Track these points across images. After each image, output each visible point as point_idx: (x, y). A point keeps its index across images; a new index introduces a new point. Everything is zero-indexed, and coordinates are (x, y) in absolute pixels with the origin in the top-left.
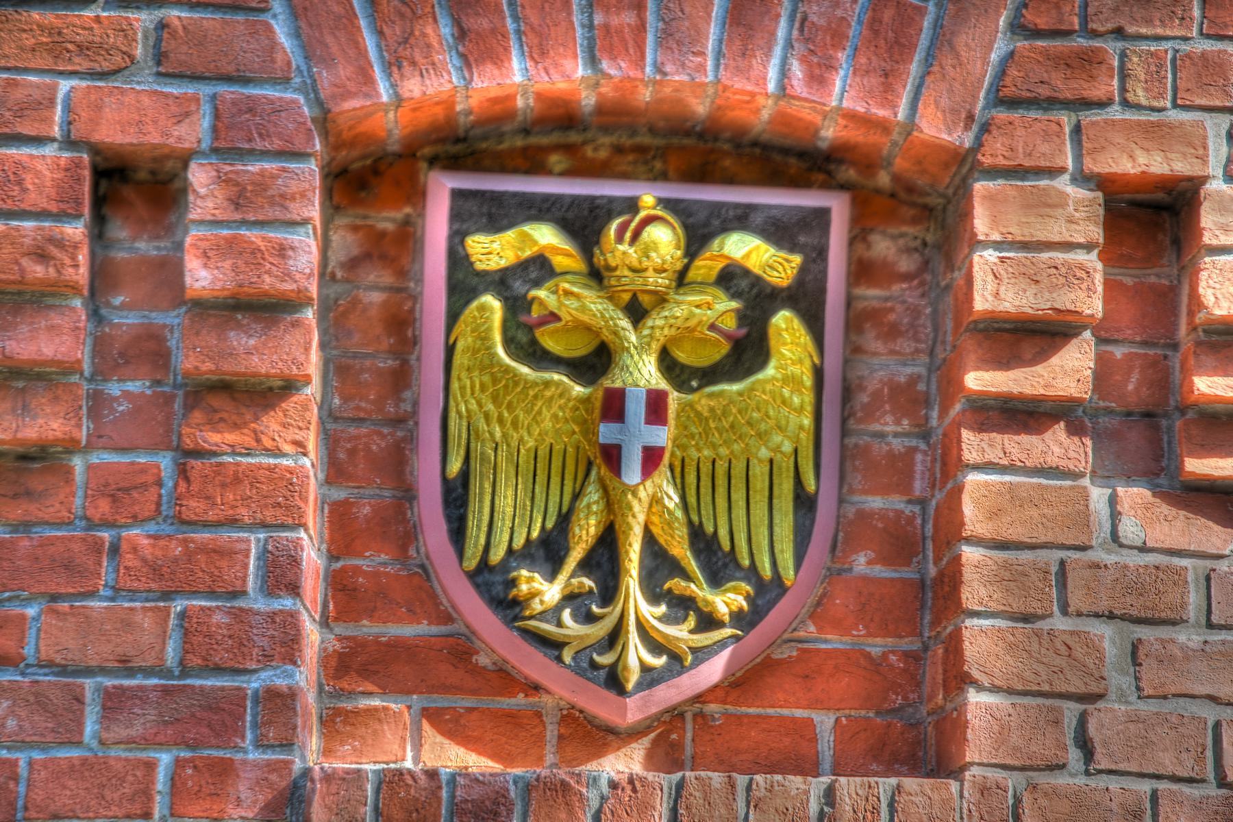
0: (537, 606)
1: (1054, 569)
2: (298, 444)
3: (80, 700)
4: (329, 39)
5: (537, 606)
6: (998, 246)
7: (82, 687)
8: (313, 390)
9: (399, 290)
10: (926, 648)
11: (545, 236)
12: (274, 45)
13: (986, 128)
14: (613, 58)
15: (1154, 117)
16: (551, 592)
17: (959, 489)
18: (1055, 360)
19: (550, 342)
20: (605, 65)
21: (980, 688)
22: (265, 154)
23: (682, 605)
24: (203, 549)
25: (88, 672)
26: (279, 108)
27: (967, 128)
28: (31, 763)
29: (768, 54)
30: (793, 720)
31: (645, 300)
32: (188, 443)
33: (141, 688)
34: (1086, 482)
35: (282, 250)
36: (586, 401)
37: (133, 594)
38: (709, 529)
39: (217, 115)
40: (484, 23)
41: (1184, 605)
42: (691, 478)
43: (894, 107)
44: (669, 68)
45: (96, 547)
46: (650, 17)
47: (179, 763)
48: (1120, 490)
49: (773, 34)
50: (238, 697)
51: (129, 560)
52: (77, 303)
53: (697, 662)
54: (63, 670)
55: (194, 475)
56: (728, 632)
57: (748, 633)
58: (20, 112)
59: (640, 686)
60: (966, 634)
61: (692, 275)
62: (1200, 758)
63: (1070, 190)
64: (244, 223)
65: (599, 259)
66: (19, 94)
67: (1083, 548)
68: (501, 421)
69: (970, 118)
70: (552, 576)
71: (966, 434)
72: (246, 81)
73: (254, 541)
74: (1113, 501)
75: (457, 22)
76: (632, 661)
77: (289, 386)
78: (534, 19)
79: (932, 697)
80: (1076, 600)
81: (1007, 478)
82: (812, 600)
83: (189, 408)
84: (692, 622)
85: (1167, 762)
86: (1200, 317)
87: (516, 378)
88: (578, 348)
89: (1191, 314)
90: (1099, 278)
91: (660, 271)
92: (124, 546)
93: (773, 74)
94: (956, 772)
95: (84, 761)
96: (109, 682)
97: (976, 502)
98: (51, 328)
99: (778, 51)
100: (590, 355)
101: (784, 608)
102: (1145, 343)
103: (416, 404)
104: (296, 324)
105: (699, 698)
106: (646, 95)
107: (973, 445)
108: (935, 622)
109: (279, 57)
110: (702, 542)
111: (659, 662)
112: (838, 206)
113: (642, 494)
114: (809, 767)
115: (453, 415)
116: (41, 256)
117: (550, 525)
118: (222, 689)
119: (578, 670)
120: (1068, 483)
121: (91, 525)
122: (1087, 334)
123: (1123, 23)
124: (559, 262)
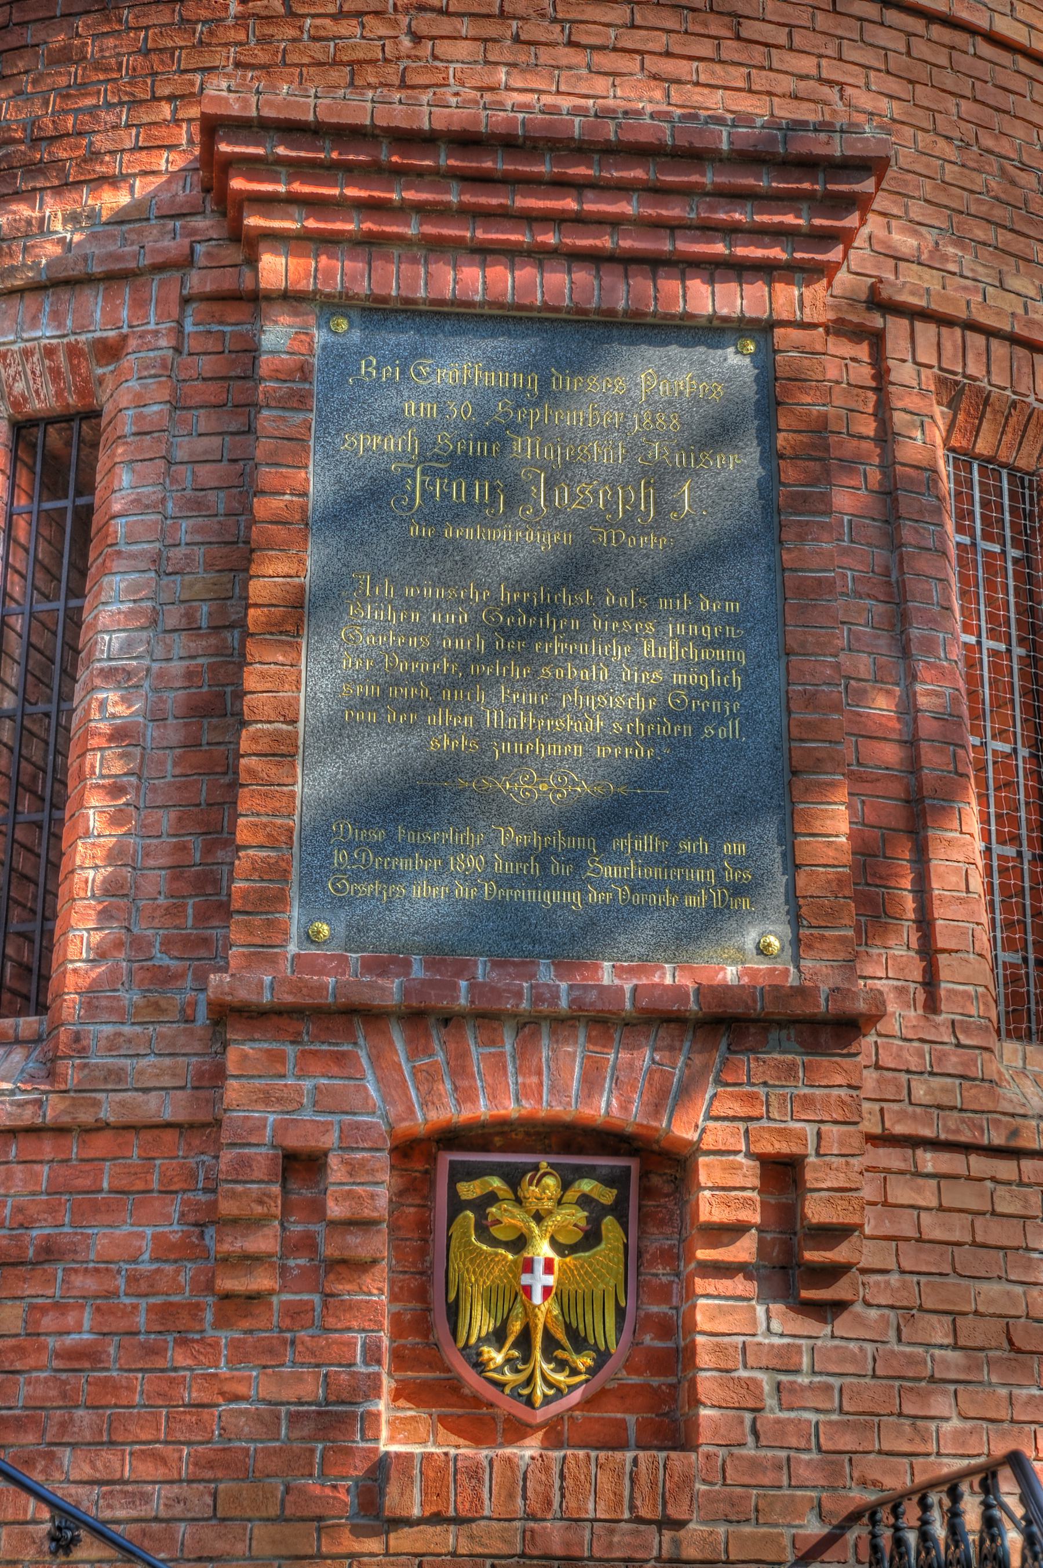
0: (492, 1366)
1: (740, 1346)
2: (379, 1289)
3: (278, 1418)
4: (393, 1093)
5: (492, 1366)
6: (711, 1189)
7: (280, 1411)
8: (384, 1263)
9: (423, 1206)
10: (679, 1382)
12: (368, 1096)
13: (704, 1131)
14: (528, 1099)
15: (783, 1125)
16: (499, 1358)
17: (694, 1306)
18: (738, 1244)
19: (495, 1231)
20: (524, 1102)
21: (705, 1406)
22: (363, 1149)
23: (562, 1365)
24: (335, 1342)
25: (282, 1404)
26: (371, 1126)
27: (695, 1131)
29: (601, 1096)
30: (616, 1419)
31: (542, 1213)
32: (328, 1290)
33: (307, 1412)
34: (754, 1302)
35: (372, 1196)
36: (515, 1262)
37: (302, 1365)
38: (574, 1325)
39: (341, 1131)
40: (466, 1083)
41: (801, 1364)
43: (661, 1121)
44: (554, 1104)
45: (284, 1342)
46: (545, 1078)
47: (324, 1448)
48: (771, 1306)
49: (603, 1086)
51: (300, 1348)
52: (276, 1223)
53: (569, 1393)
54: (270, 1403)
55: (330, 1306)
56: (583, 1377)
58: (251, 1131)
59: (543, 1404)
60: (699, 1380)
61: (564, 1200)
62: (809, 1440)
63: (744, 1161)
64: (354, 1183)
65: (520, 1193)
66: (250, 1124)
67: (754, 1335)
68: (474, 1272)
69: (697, 1126)
70: (499, 1350)
71: (697, 1279)
72: (355, 1114)
73: (360, 1338)
74: (768, 1311)
75: (454, 1083)
76: (539, 1393)
77: (375, 1262)
78: (490, 1081)
79: (683, 1407)
80: (751, 1361)
81: (717, 1302)
82: (624, 1359)
83: (327, 1273)
84: (567, 1372)
85: (794, 1442)
86: (805, 1223)
87: (481, 1252)
88: (511, 1236)
89: (802, 1220)
90: (758, 1204)
91: (550, 1199)
92: (298, 1341)
93: (603, 1105)
94: (694, 1448)
95: (281, 1448)
96: (293, 1408)
97: (703, 1313)
98: (264, 1236)
99: (605, 1094)
101: (611, 1362)
102: (781, 1232)
103: (432, 1263)
104: (378, 1231)
105: (571, 1409)
106: (543, 1114)
107: (701, 1285)
108: (684, 1370)
109: (370, 1102)
110: (572, 1332)
111: (551, 1392)
112: (633, 1164)
113: (543, 1308)
114: (623, 1446)
115: (451, 1270)
116: (261, 1202)
119: (512, 1396)
120: (745, 1303)
121: (281, 1331)
122: (753, 1231)
123: (767, 1079)
124: (501, 1194)
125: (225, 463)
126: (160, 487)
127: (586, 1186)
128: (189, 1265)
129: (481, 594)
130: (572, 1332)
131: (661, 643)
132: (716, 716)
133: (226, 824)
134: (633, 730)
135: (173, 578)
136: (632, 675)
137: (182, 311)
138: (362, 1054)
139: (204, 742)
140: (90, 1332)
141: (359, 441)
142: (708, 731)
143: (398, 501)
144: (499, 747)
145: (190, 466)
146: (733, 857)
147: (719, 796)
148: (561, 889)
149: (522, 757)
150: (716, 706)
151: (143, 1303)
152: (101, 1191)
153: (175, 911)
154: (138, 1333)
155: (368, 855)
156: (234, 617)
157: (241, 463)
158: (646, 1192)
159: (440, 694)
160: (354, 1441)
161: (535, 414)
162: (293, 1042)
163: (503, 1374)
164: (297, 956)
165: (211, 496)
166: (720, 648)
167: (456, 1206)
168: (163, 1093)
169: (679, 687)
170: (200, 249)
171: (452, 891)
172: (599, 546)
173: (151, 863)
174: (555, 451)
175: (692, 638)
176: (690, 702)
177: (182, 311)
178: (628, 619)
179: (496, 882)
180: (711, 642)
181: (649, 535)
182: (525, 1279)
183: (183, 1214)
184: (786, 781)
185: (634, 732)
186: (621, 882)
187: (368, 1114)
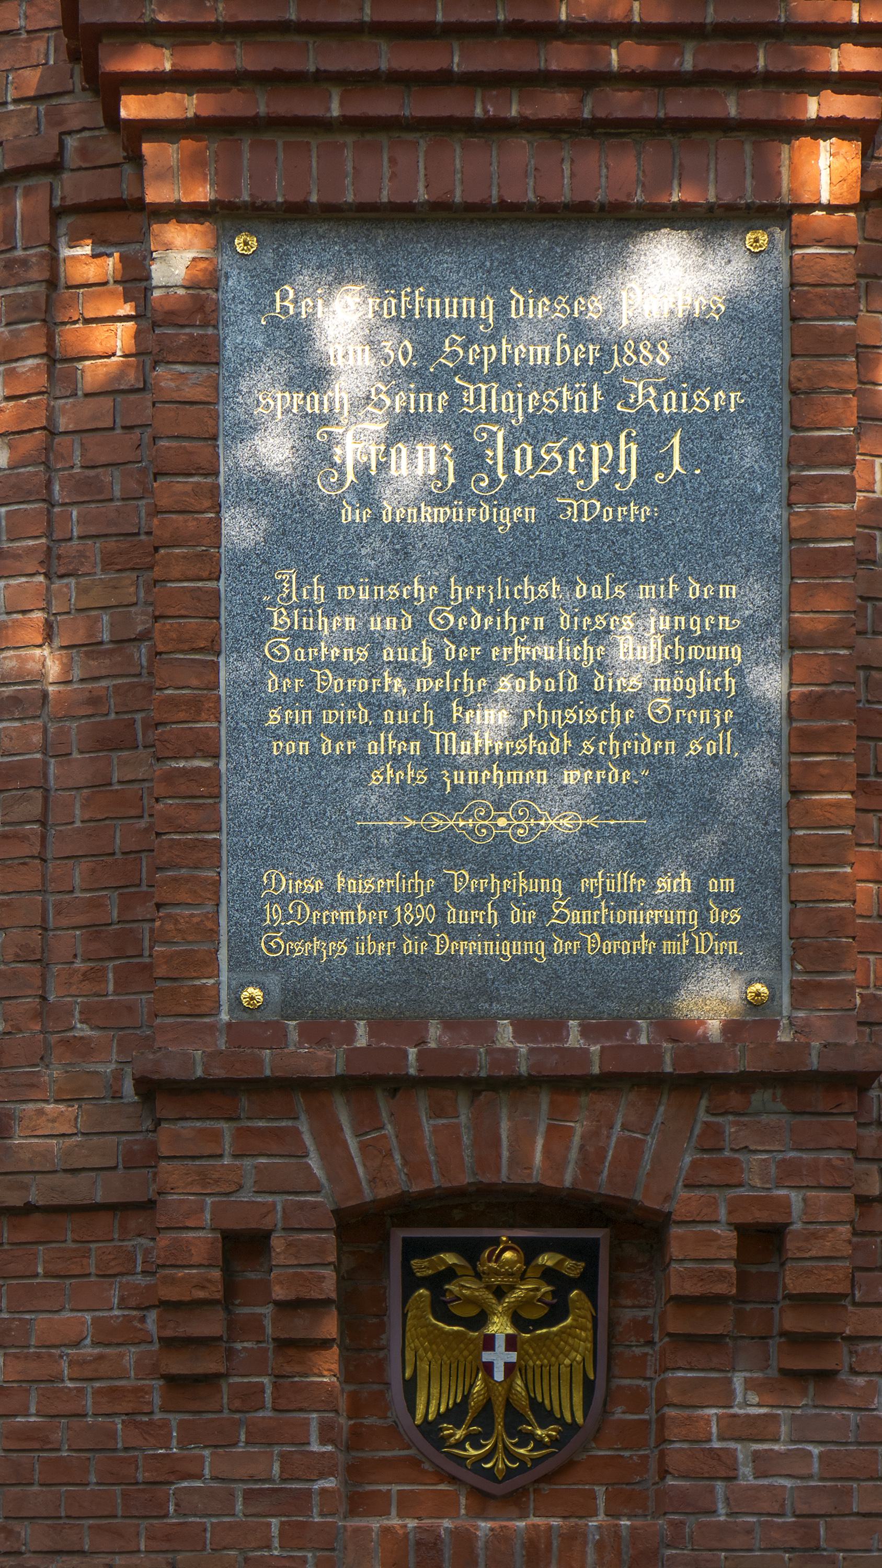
11: (450, 1259)
28: (212, 1524)
38: (540, 1400)
42: (530, 1376)
47: (282, 1523)
50: (309, 1492)
57: (560, 1450)
100: (477, 1315)
103: (388, 1340)
117: (458, 1401)
118: (300, 1489)
125: (119, 431)
126: (42, 468)
127: (547, 1260)
128: (133, 1350)
129: (427, 590)
130: (536, 1406)
131: (641, 639)
132: (704, 728)
133: (144, 875)
134: (606, 749)
135: (65, 581)
136: (606, 683)
137: (54, 226)
138: (304, 1127)
139: (115, 780)
140: (37, 1415)
141: (275, 399)
142: (694, 747)
143: (327, 475)
144: (451, 777)
145: (76, 437)
146: (718, 895)
147: (704, 824)
148: (522, 939)
149: (475, 787)
150: (704, 716)
151: (89, 1387)
152: (36, 1275)
153: (94, 976)
154: (85, 1415)
155: (303, 908)
156: (140, 628)
157: (138, 431)
158: (617, 1264)
159: (381, 716)
160: (312, 1517)
161: (490, 352)
162: (229, 1119)
163: (466, 1450)
164: (229, 1025)
165: (106, 476)
166: (711, 644)
167: (411, 1283)
168: (93, 1174)
169: (660, 694)
170: (71, 143)
171: (399, 946)
172: (568, 523)
173: (65, 922)
174: (515, 400)
175: (678, 633)
176: (674, 712)
177: (54, 226)
178: (601, 613)
179: (448, 934)
180: (700, 637)
181: (628, 504)
182: (487, 1356)
183: (122, 1299)
184: (785, 801)
185: (607, 752)
186: (590, 929)
187: (311, 1193)
